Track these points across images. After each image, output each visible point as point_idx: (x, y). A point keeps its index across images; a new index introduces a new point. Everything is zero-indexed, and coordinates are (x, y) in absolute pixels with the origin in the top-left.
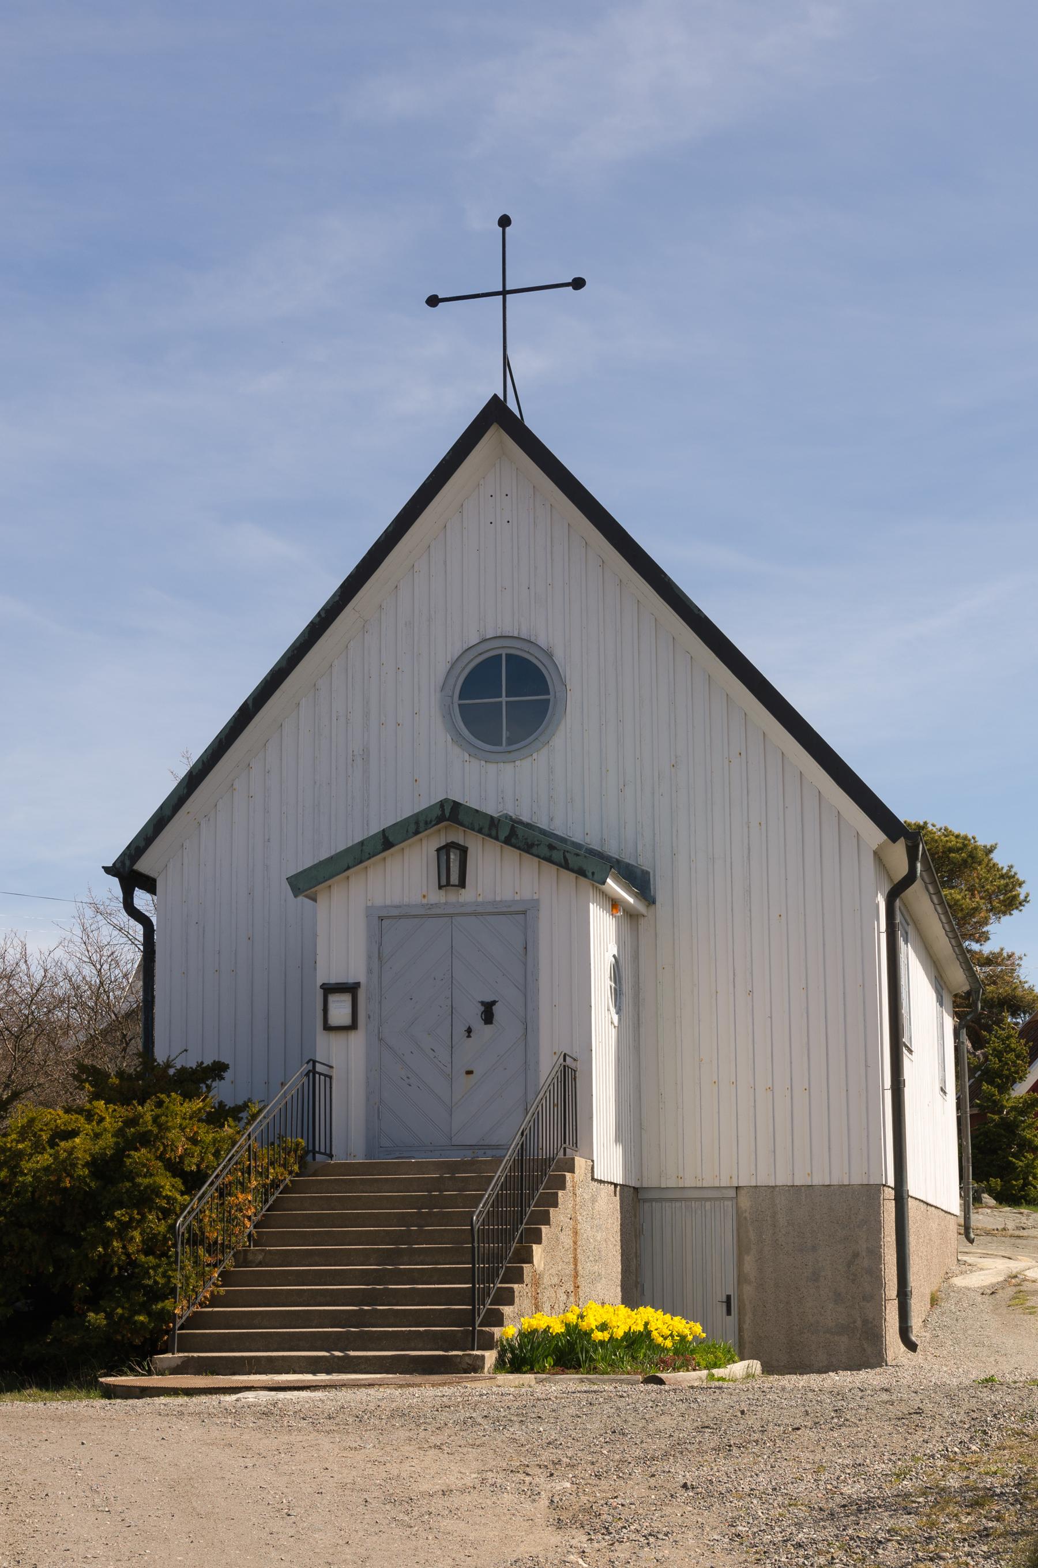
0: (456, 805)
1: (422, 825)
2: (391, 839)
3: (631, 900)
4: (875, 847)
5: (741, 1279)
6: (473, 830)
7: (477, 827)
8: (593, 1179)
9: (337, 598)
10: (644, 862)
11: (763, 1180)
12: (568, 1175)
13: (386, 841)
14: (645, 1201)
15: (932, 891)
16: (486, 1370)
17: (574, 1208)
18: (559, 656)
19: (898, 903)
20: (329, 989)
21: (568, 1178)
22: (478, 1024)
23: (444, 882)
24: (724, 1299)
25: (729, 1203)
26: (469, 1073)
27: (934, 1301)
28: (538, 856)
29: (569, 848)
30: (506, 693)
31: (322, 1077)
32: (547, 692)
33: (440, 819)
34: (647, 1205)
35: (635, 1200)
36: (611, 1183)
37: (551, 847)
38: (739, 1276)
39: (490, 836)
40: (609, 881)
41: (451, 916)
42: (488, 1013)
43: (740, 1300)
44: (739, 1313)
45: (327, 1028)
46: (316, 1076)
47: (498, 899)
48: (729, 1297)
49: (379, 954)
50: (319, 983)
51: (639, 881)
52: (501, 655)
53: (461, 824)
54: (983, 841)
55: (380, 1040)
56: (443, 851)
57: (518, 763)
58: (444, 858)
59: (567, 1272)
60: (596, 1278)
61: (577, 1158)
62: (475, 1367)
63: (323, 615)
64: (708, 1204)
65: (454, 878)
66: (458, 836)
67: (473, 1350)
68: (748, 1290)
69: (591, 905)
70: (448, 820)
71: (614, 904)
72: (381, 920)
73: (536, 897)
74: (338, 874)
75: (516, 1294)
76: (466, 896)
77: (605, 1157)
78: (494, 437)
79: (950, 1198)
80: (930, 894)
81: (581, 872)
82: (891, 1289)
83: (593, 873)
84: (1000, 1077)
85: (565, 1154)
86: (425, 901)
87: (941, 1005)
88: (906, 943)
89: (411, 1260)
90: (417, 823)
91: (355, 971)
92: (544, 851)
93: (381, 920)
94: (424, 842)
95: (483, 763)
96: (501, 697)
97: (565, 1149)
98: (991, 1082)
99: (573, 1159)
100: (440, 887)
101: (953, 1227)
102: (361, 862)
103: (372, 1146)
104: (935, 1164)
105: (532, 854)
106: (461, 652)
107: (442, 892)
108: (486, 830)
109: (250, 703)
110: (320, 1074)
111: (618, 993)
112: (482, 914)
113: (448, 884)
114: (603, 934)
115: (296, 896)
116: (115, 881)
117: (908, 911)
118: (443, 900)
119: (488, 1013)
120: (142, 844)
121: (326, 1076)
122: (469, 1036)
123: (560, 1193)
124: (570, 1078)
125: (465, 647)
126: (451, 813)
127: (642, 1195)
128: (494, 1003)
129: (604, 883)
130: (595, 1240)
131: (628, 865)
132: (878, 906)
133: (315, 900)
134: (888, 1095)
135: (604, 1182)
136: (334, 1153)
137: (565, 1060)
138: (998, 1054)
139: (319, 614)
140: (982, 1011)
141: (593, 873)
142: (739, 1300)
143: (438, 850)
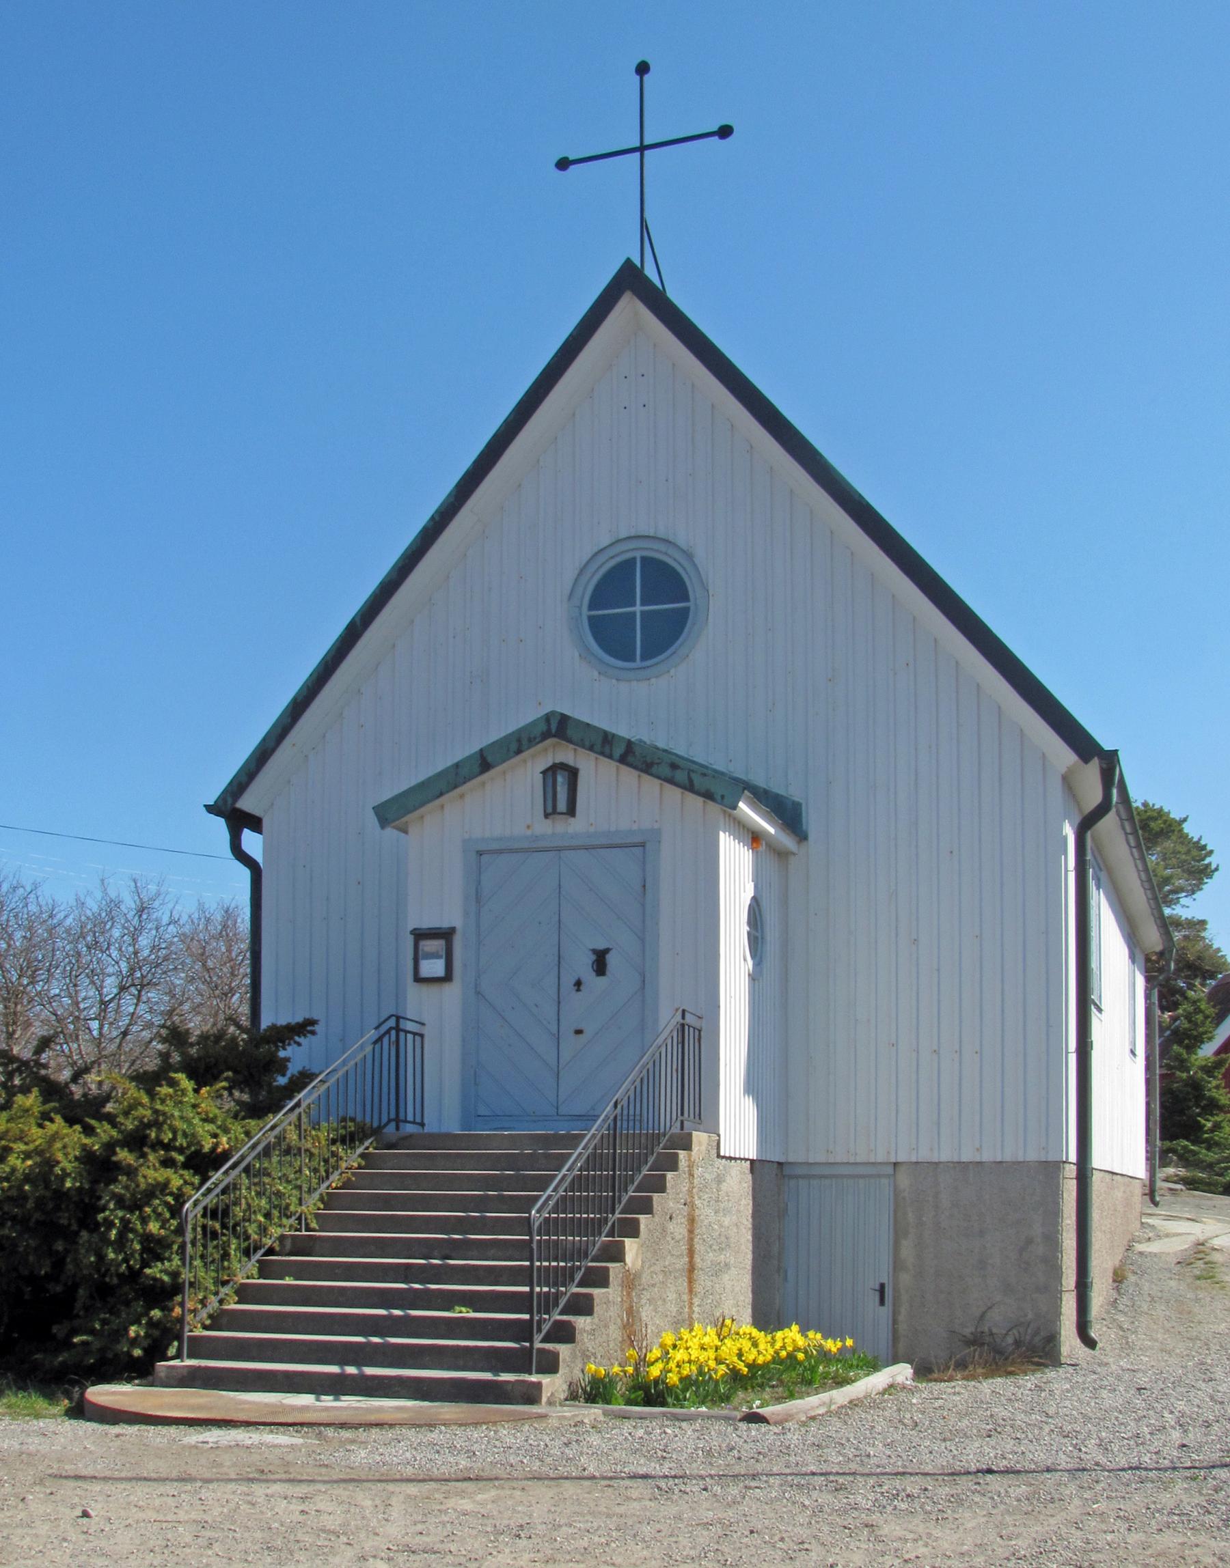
0: (564, 719)
1: (525, 742)
2: (489, 759)
3: (772, 830)
4: (1063, 770)
5: (897, 1265)
6: (583, 747)
7: (587, 744)
8: (719, 1156)
9: (452, 500)
10: (794, 792)
11: (924, 1155)
12: (682, 1154)
13: (484, 762)
14: (791, 1177)
15: (1128, 829)
16: (544, 1399)
17: (690, 1191)
18: (700, 555)
19: (1089, 834)
20: (420, 935)
21: (681, 1157)
22: (588, 975)
23: (550, 810)
24: (877, 1287)
25: (885, 1181)
26: (579, 1032)
27: (1118, 1278)
28: (659, 778)
29: (694, 767)
30: (639, 606)
31: (410, 1036)
32: (686, 598)
33: (546, 735)
34: (793, 1183)
35: (772, 1177)
36: (747, 1160)
37: (674, 766)
38: (895, 1262)
39: (602, 754)
40: (741, 805)
41: (559, 849)
42: (600, 963)
43: (896, 1290)
44: (894, 1305)
45: (418, 979)
46: (395, 1031)
47: (613, 829)
48: (882, 1286)
49: (477, 898)
50: (410, 927)
51: (788, 814)
52: (634, 559)
53: (570, 741)
54: (1175, 815)
55: (478, 993)
56: (551, 772)
57: (653, 680)
58: (550, 781)
59: (678, 1266)
60: (719, 1269)
61: (695, 1133)
62: (531, 1395)
63: (437, 518)
64: (861, 1181)
65: (562, 806)
66: (566, 754)
67: (530, 1374)
68: (905, 1278)
69: (721, 834)
70: (554, 736)
71: (754, 838)
72: (480, 855)
73: (656, 826)
74: (429, 801)
75: (596, 1301)
76: (576, 826)
77: (738, 1126)
78: (629, 307)
79: (1136, 1165)
80: (1126, 834)
81: (708, 796)
82: (1069, 1279)
83: (723, 797)
84: (1189, 1037)
85: (682, 1128)
86: (529, 832)
87: (1133, 962)
88: (1098, 889)
89: (480, 1257)
90: (519, 741)
91: (450, 915)
92: (665, 770)
93: (480, 855)
94: (529, 764)
95: (614, 681)
96: (642, 613)
97: (682, 1123)
98: (1180, 1043)
99: (690, 1135)
100: (547, 816)
101: (1138, 1190)
102: (456, 787)
103: (469, 1116)
104: (1122, 1133)
105: (651, 775)
106: (590, 556)
107: (549, 822)
108: (598, 747)
109: (358, 620)
110: (407, 1032)
111: (756, 942)
112: (594, 847)
113: (554, 812)
114: (736, 871)
115: (383, 827)
116: (221, 822)
117: (1101, 855)
118: (550, 831)
119: (600, 963)
120: (244, 779)
121: (415, 1034)
122: (578, 990)
123: (670, 1175)
124: (694, 1038)
125: (596, 549)
126: (559, 727)
127: (787, 1171)
128: (607, 951)
129: (735, 807)
130: (721, 1226)
131: (777, 796)
132: (1065, 838)
133: (406, 832)
134: (1073, 1058)
135: (735, 1159)
136: (426, 1121)
137: (683, 1018)
138: (1188, 1017)
139: (433, 518)
140: (1174, 972)
141: (723, 797)
142: (894, 1289)
143: (544, 773)
